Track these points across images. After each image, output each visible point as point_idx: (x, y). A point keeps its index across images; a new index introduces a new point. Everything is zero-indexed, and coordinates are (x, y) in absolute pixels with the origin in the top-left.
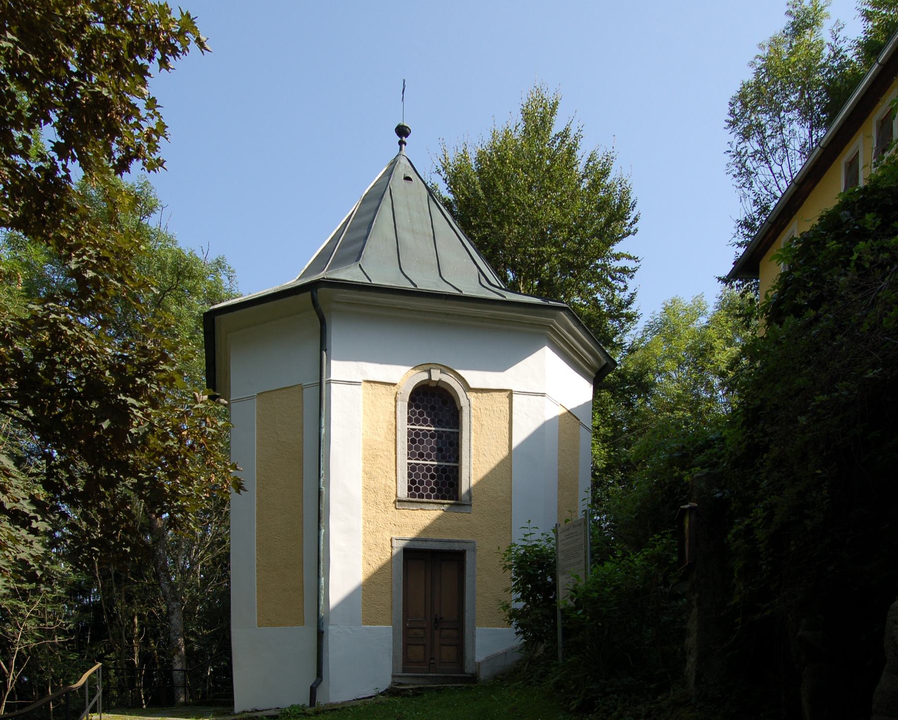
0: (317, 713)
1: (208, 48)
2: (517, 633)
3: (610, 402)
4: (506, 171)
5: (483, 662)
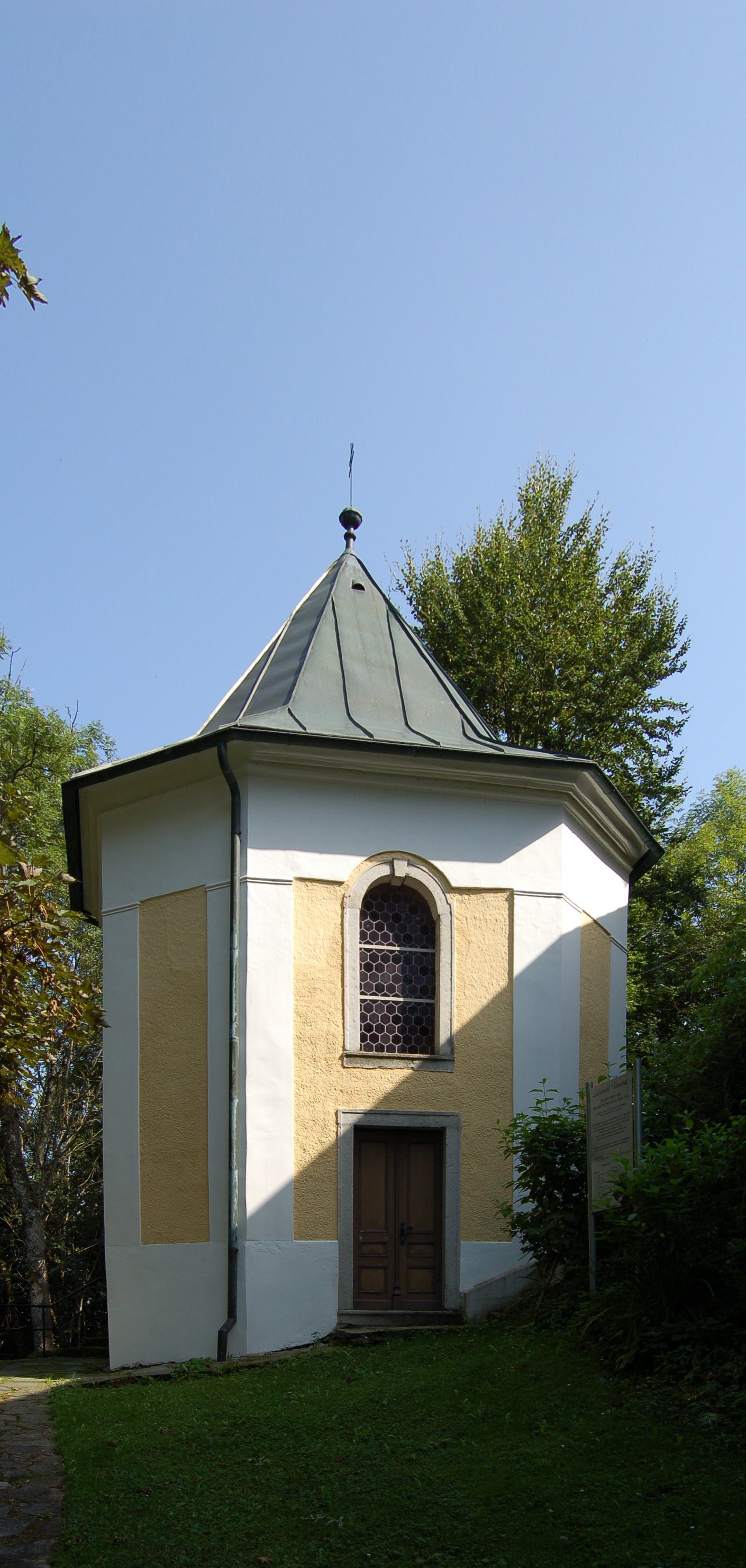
0: (228, 1372)
1: (41, 296)
2: (524, 1250)
3: (645, 916)
4: (498, 580)
5: (471, 1292)
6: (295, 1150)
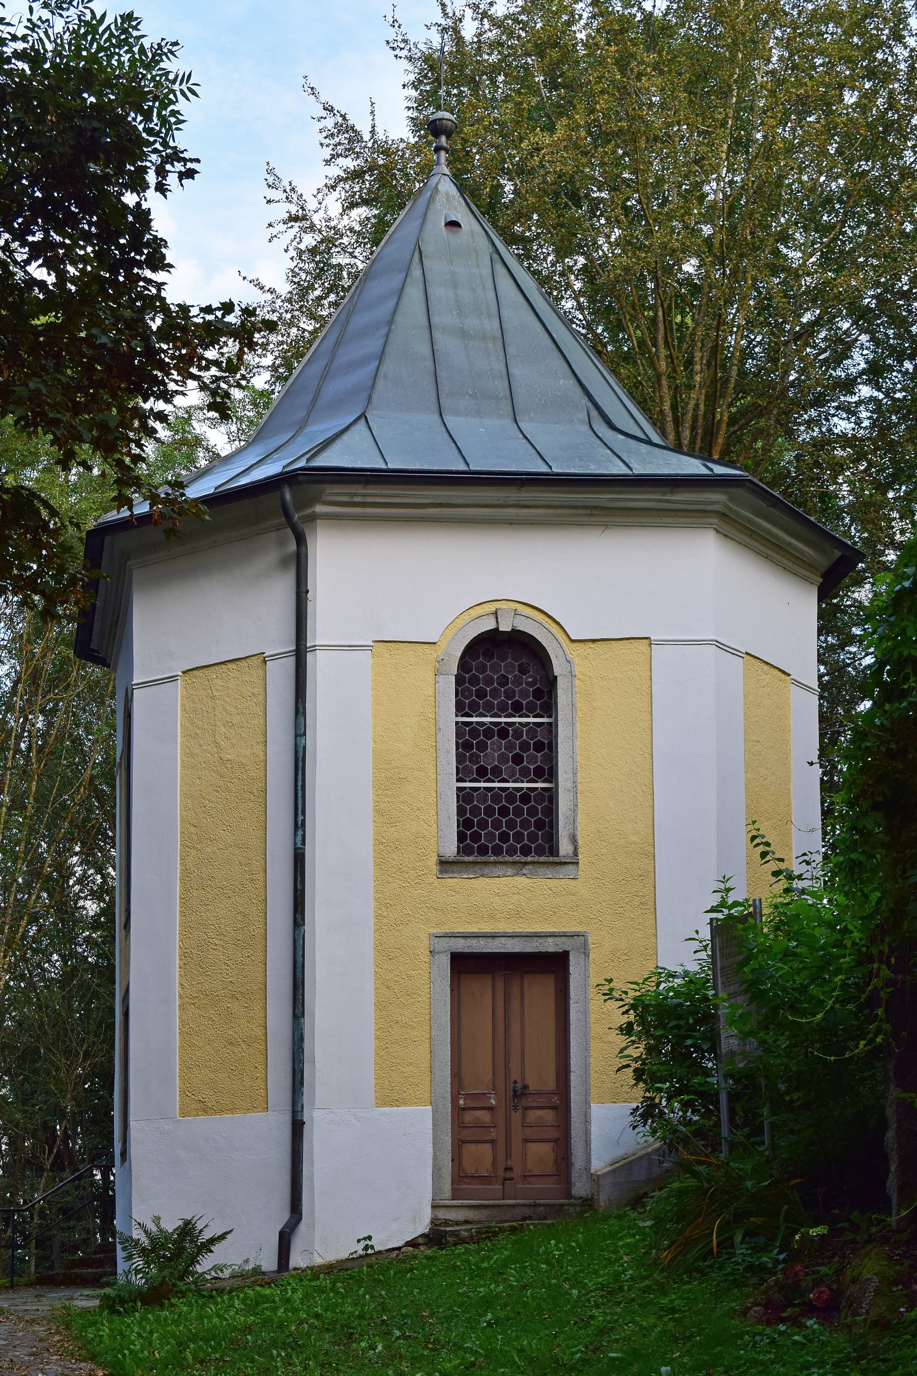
6: (376, 989)
